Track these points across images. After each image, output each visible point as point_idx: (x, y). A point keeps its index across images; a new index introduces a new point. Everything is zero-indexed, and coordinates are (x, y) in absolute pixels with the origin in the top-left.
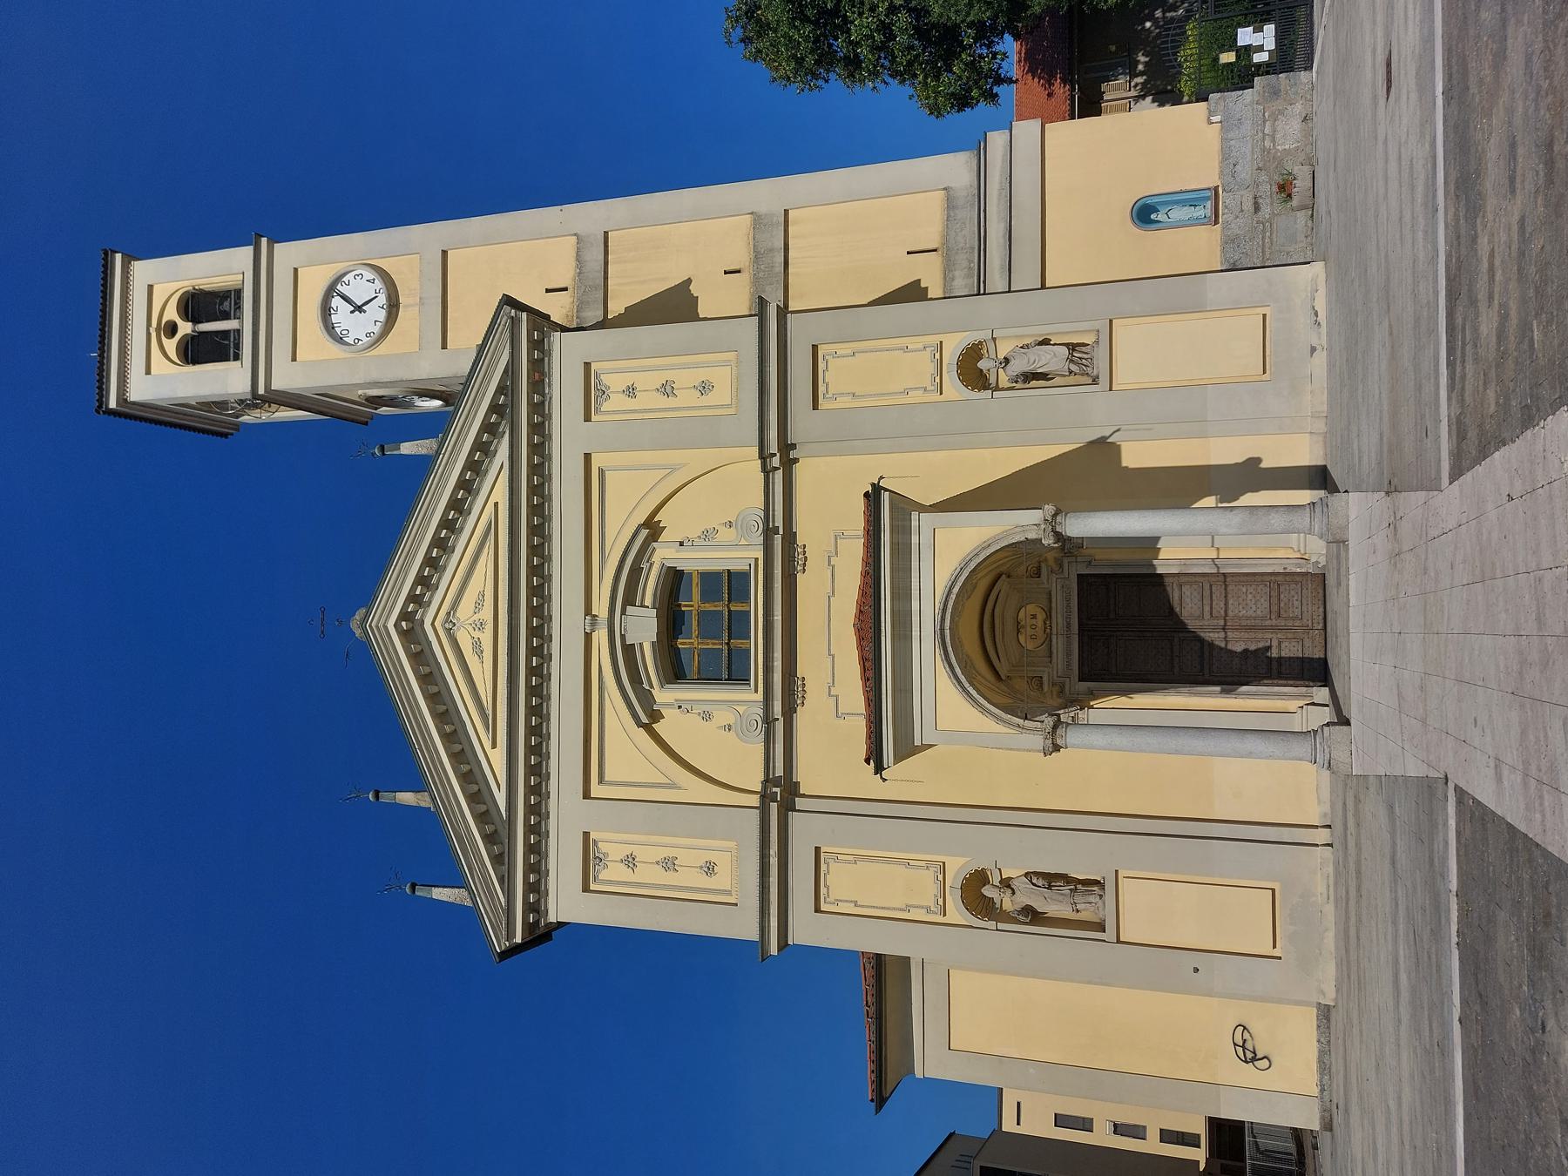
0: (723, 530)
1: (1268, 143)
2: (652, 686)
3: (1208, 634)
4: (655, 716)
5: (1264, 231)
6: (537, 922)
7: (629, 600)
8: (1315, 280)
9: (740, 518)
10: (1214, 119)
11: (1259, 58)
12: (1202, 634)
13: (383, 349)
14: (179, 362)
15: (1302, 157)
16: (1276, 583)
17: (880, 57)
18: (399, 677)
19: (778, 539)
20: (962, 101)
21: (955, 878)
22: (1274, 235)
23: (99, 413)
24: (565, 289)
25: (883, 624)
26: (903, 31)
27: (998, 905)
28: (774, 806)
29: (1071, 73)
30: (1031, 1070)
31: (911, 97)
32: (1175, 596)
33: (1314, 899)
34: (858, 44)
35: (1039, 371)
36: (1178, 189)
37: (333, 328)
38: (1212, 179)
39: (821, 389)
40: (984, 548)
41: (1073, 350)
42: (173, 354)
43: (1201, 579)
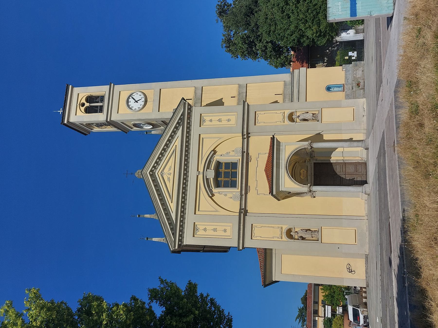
0: (231, 152)
1: (355, 75)
2: (212, 188)
3: (342, 176)
4: (213, 195)
5: (354, 93)
6: (181, 244)
7: (208, 168)
8: (364, 102)
9: (236, 150)
10: (343, 70)
11: (353, 58)
12: (341, 176)
13: (142, 111)
14: (85, 113)
15: (362, 78)
16: (356, 164)
17: (263, 53)
18: (150, 185)
19: (245, 154)
20: (283, 65)
21: (285, 230)
22: (356, 94)
23: (61, 124)
24: (191, 99)
25: (274, 164)
26: (269, 48)
27: (294, 237)
28: (242, 214)
29: (308, 61)
30: (301, 277)
31: (268, 64)
32: (335, 168)
33: (364, 231)
34: (258, 50)
35: (306, 119)
36: (336, 84)
37: (129, 106)
38: (343, 82)
39: (257, 121)
40: (296, 149)
41: (314, 115)
42: (83, 111)
43: (340, 164)
